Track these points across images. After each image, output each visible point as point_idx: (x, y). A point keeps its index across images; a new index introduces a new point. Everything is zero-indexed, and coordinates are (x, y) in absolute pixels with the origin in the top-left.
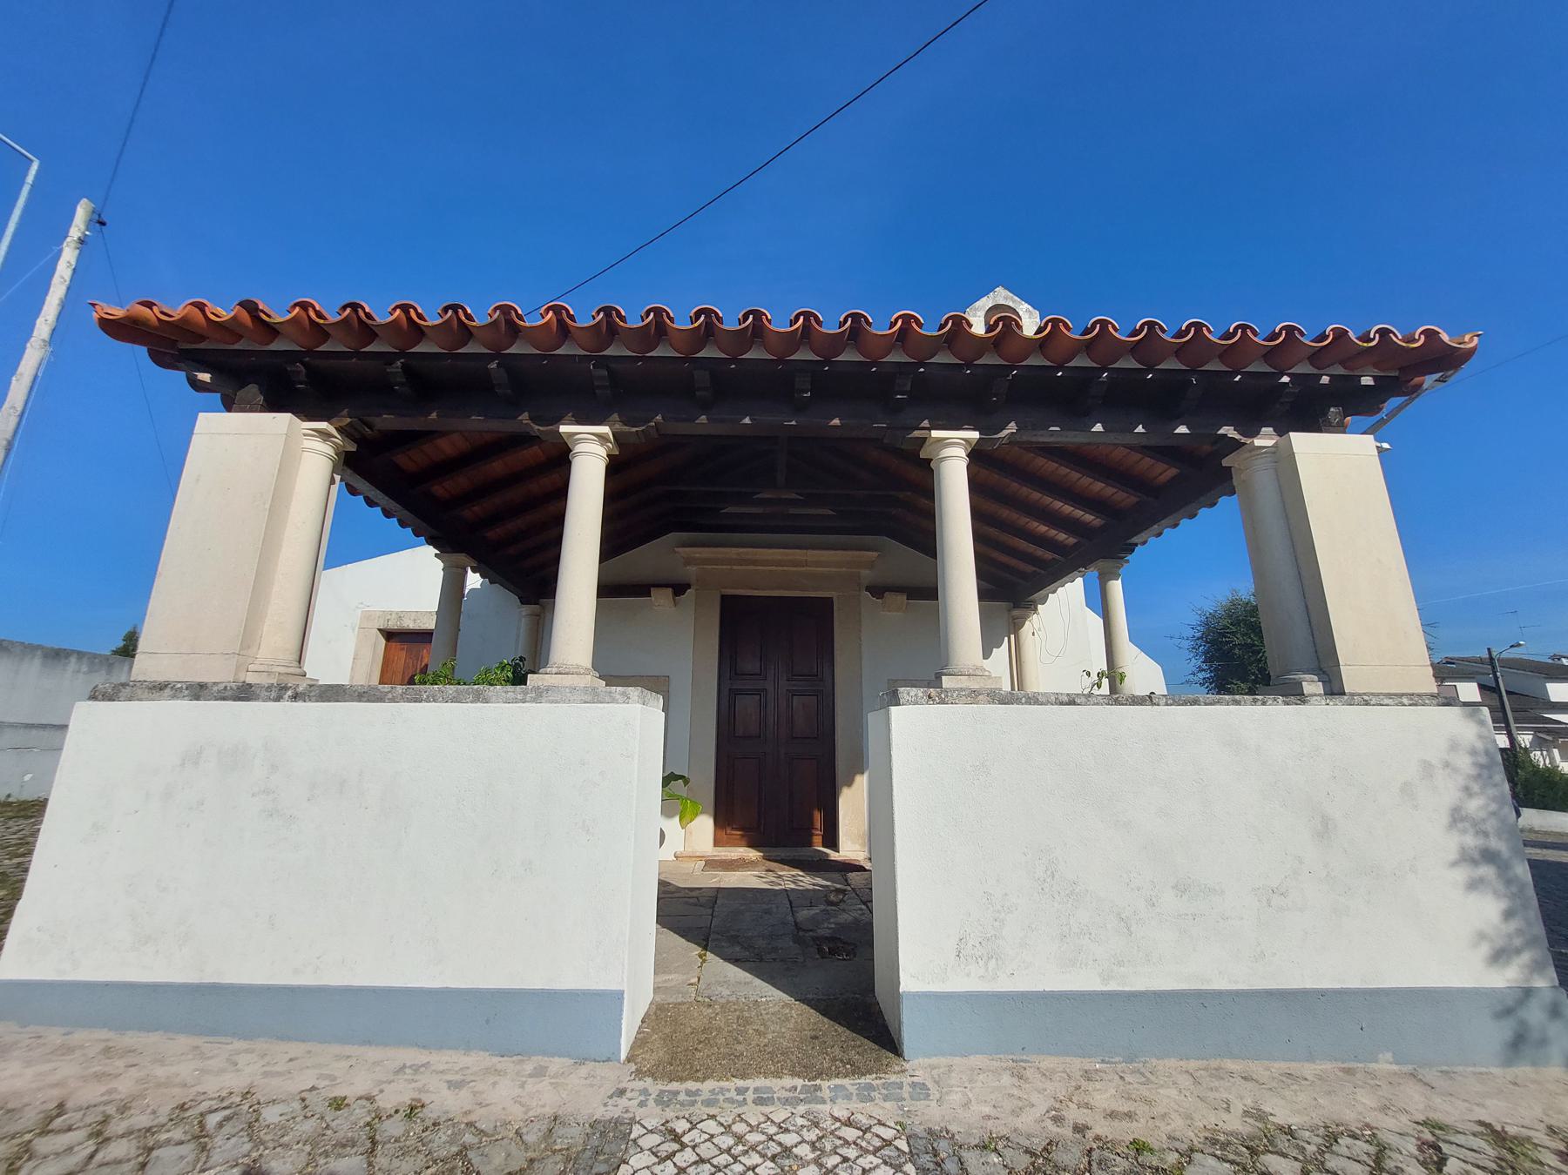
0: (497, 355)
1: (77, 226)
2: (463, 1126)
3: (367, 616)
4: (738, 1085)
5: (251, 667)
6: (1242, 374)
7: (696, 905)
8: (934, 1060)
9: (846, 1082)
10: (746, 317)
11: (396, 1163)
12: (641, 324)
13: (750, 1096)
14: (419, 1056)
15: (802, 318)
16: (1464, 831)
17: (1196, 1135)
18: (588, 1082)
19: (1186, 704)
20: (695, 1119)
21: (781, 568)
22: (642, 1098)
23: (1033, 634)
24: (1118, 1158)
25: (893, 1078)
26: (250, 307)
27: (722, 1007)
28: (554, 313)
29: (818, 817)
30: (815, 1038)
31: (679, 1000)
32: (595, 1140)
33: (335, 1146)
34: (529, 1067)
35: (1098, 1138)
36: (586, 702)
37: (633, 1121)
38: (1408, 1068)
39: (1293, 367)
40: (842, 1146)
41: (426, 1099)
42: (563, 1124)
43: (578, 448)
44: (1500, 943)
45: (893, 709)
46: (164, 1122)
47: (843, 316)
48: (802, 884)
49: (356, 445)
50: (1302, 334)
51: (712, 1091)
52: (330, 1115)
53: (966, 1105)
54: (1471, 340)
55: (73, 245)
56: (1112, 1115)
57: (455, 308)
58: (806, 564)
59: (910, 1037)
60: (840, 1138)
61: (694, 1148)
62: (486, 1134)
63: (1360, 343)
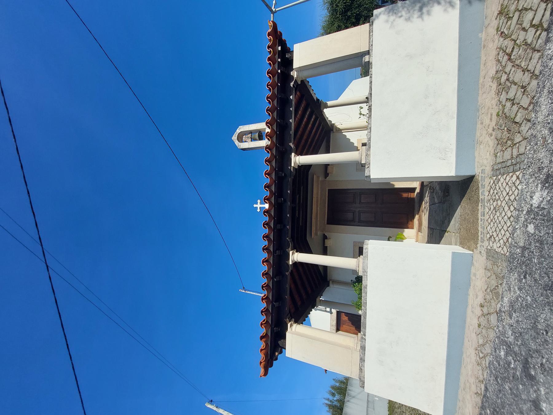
0: (273, 278)
1: (213, 408)
2: (486, 292)
4: (480, 221)
5: (355, 348)
6: (278, 83)
7: (433, 234)
8: (476, 166)
9: (480, 191)
10: (265, 215)
11: (493, 307)
12: (267, 241)
13: (483, 218)
14: (470, 307)
15: (265, 201)
16: (413, 17)
17: (496, 98)
18: (477, 262)
19: (371, 96)
20: (487, 232)
21: (319, 206)
22: (482, 247)
23: (342, 124)
24: (500, 122)
25: (480, 178)
26: (262, 338)
27: (461, 226)
28: (264, 262)
29: (405, 195)
30: (470, 199)
31: (459, 238)
32: (490, 258)
33: (488, 323)
34: (474, 278)
35: (496, 125)
36: (368, 259)
37: (487, 249)
38: (484, 29)
39: (276, 69)
40: (494, 194)
41: (479, 304)
42: (486, 267)
43: (296, 260)
44: (448, 5)
45: (371, 177)
46: (481, 367)
47: (265, 190)
48: (427, 201)
49: (293, 319)
50: (269, 70)
51: (481, 228)
52: (482, 327)
53: (487, 159)
54: (270, 23)
55: (218, 410)
56: (491, 119)
57: (263, 287)
58: (317, 198)
59: (469, 173)
60: (493, 194)
61: (493, 232)
62: (488, 286)
63: (272, 54)
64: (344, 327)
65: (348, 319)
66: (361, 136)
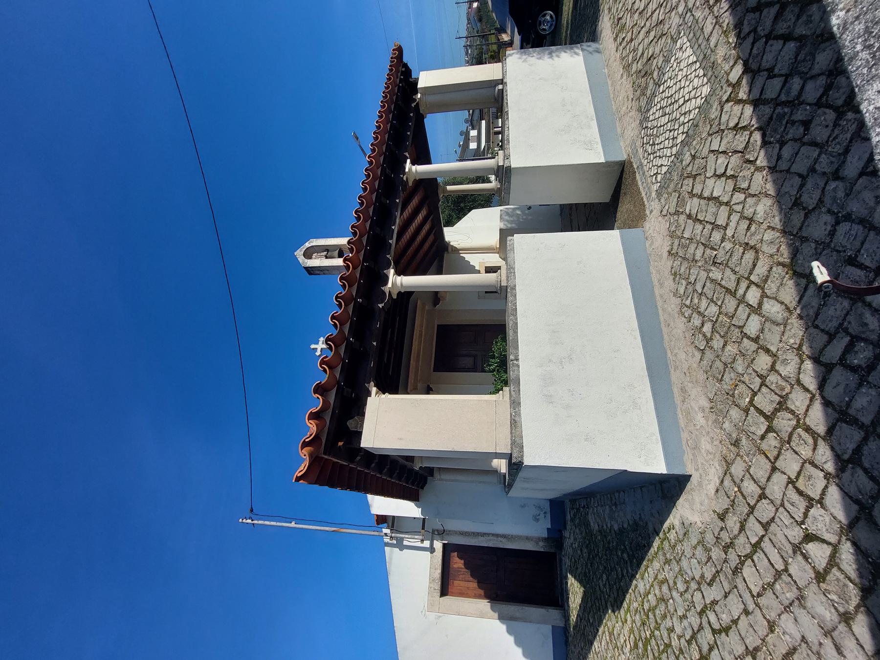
3: (431, 607)
64: (456, 584)
65: (465, 564)
66: (483, 259)
